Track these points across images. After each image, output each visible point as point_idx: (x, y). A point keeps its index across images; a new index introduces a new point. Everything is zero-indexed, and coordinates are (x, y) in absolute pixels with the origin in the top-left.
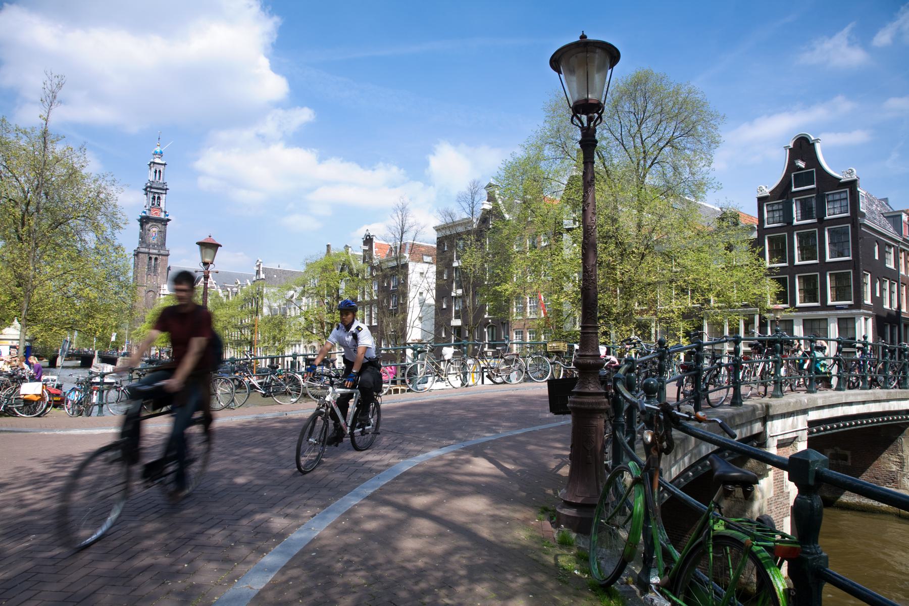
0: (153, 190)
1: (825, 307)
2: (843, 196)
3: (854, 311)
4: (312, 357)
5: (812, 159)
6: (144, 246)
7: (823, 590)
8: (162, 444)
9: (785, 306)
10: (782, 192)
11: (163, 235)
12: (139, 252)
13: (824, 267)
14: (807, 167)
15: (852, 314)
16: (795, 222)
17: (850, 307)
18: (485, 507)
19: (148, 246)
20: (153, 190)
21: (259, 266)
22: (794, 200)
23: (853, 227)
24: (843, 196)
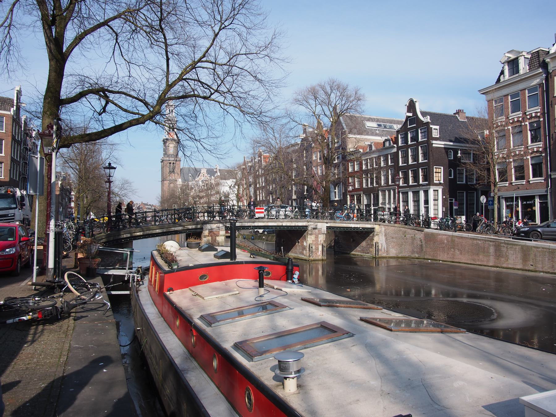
1: (409, 186)
3: (428, 187)
10: (404, 130)
12: (163, 160)
14: (413, 115)
15: (427, 188)
16: (409, 143)
17: (427, 185)
19: (168, 156)
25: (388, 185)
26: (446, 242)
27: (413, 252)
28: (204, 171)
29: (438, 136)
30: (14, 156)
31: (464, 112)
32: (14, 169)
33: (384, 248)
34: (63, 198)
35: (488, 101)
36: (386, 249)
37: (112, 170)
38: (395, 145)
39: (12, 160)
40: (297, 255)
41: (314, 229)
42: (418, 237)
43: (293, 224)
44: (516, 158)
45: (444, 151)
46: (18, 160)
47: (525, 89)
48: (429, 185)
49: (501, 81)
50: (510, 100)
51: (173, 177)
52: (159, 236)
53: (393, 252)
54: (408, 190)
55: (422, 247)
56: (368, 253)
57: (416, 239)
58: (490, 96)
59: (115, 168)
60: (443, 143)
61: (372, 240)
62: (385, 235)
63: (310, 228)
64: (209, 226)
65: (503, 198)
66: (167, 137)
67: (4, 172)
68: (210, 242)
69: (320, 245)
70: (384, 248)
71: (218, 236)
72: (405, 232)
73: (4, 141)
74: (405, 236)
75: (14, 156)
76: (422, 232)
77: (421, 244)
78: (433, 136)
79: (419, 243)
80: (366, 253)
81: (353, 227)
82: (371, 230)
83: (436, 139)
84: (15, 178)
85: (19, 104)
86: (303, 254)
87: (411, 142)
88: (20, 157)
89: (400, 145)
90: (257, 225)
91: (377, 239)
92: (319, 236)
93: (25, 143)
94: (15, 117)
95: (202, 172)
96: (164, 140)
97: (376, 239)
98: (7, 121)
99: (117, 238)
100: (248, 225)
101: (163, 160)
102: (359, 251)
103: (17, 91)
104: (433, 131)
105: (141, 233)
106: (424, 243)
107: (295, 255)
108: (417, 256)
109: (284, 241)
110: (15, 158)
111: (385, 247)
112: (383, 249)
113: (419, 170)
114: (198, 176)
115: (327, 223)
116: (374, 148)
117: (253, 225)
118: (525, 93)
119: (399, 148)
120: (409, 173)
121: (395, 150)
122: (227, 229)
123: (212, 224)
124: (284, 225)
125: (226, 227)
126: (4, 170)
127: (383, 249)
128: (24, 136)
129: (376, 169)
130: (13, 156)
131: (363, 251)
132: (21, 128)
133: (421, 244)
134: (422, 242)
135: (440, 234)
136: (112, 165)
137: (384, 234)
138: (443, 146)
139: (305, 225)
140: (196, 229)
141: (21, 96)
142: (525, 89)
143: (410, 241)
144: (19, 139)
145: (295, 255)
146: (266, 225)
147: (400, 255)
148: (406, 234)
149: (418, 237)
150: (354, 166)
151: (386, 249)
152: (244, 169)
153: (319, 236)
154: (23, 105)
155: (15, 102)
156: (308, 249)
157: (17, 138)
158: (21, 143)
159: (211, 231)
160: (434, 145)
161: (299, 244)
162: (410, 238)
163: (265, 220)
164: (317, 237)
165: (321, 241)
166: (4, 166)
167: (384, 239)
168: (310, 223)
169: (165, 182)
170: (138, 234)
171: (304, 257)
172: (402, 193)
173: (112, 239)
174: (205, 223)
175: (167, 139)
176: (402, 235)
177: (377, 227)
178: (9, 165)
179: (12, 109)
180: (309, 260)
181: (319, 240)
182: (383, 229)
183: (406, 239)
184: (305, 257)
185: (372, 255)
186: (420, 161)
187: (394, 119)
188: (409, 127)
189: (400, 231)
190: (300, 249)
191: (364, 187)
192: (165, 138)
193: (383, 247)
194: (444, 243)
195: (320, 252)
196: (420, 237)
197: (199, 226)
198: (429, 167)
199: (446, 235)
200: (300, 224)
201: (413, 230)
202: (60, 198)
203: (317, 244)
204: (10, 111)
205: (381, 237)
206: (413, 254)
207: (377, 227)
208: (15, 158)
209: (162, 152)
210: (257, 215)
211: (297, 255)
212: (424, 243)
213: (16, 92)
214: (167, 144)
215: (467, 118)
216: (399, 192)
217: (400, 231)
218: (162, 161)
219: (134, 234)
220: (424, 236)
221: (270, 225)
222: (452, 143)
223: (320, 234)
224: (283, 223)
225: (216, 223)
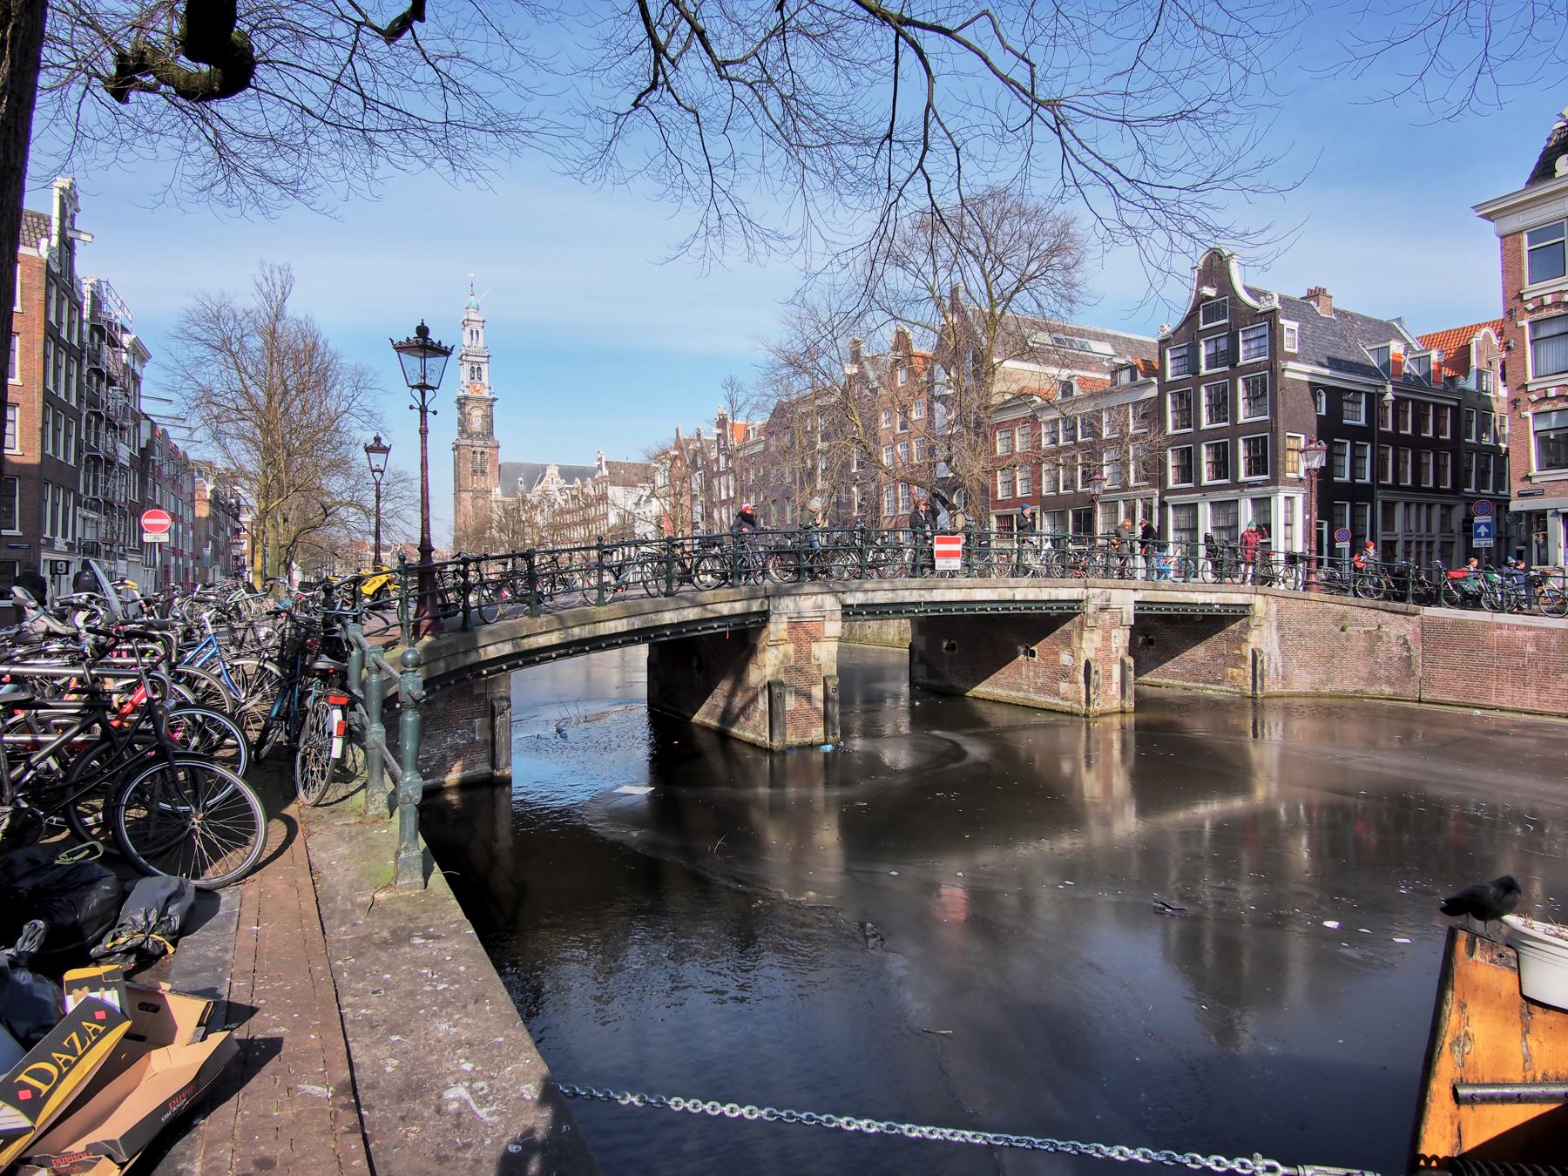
0: (469, 358)
1: (1200, 488)
2: (1261, 332)
3: (1270, 488)
4: (1100, 528)
5: (1226, 286)
6: (465, 436)
7: (460, 909)
8: (764, 650)
9: (1264, 477)
10: (1188, 334)
11: (489, 419)
12: (458, 446)
13: (1237, 430)
14: (1219, 295)
15: (1266, 492)
16: (1203, 371)
17: (1266, 483)
18: (446, 780)
19: (470, 436)
20: (469, 358)
21: (600, 459)
22: (1202, 343)
23: (1271, 373)
24: (1261, 332)
25: (1125, 487)
26: (1530, 649)
27: (1373, 678)
28: (552, 471)
29: (1296, 351)
30: (56, 387)
31: (1328, 293)
32: (56, 430)
33: (1276, 668)
34: (218, 528)
35: (1503, 237)
36: (1280, 670)
37: (434, 363)
38: (1154, 380)
39: (49, 399)
40: (1021, 694)
41: (1103, 609)
42: (1393, 633)
43: (1044, 594)
44: (1545, 407)
45: (1307, 391)
46: (73, 403)
47: (1521, 232)
48: (1274, 481)
49: (1557, 175)
50: (1526, 247)
51: (480, 483)
52: (617, 645)
53: (1303, 682)
54: (1235, 495)
55: (1410, 665)
56: (1218, 682)
57: (1385, 639)
58: (1512, 223)
59: (446, 353)
60: (1309, 368)
61: (1241, 640)
62: (1280, 627)
63: (1090, 609)
64: (787, 604)
65: (1556, 513)
66: (467, 393)
67: (21, 435)
68: (792, 663)
69: (1115, 662)
70: (1276, 668)
71: (817, 640)
72: (1343, 617)
73: (17, 338)
74: (1343, 630)
75: (56, 387)
76: (1411, 618)
77: (1405, 654)
78: (1286, 349)
79: (1396, 650)
80: (1206, 682)
81: (1200, 602)
82: (1240, 614)
83: (1293, 357)
84: (61, 457)
85: (70, 234)
86: (1057, 694)
87: (1207, 368)
88: (80, 397)
89: (1169, 377)
90: (938, 599)
91: (1257, 639)
92: (1114, 633)
93: (96, 357)
94: (56, 269)
95: (548, 472)
96: (459, 400)
97: (1254, 639)
98: (29, 276)
99: (461, 664)
100: (913, 600)
101: (458, 446)
102: (1174, 676)
103: (62, 189)
104: (1286, 335)
105: (554, 639)
106: (1417, 651)
107: (1014, 694)
108: (1388, 690)
109: (951, 648)
110: (62, 395)
111: (1280, 665)
112: (1272, 671)
113: (1200, 449)
114: (539, 483)
115: (1135, 590)
116: (1077, 391)
117: (929, 599)
118: (1520, 241)
119: (1164, 387)
120: (1199, 459)
121: (1152, 392)
122: (847, 614)
123: (800, 595)
124: (1018, 597)
125: (844, 606)
126: (21, 429)
127: (1272, 671)
128: (92, 337)
129: (1083, 446)
130: (51, 387)
131: (1195, 675)
132: (81, 310)
133: (1405, 654)
134: (1409, 650)
135: (1500, 626)
136: (434, 336)
137: (1275, 624)
138: (1306, 378)
139: (1075, 598)
140: (746, 615)
141: (78, 210)
142: (1521, 232)
143: (1362, 644)
144: (75, 342)
145: (1014, 694)
146: (968, 598)
147: (1326, 690)
148: (1346, 623)
149: (1393, 633)
150: (1012, 438)
151: (1280, 670)
152: (676, 457)
153: (1114, 633)
154: (83, 237)
155: (56, 223)
156: (1081, 678)
157: (64, 335)
158: (82, 357)
159: (795, 624)
160: (1288, 374)
161: (1036, 659)
162: (1363, 636)
163: (955, 581)
164: (1107, 638)
165: (1117, 649)
166: (21, 415)
167: (1275, 636)
168: (1092, 591)
169: (463, 495)
170: (543, 641)
171: (1060, 702)
172: (1174, 506)
173: (441, 668)
174: (779, 593)
175: (466, 398)
176: (1332, 626)
177: (1258, 602)
178: (38, 415)
179: (44, 242)
180: (1086, 716)
181: (1114, 645)
182: (1274, 607)
183: (1347, 640)
184: (1068, 703)
185: (1237, 690)
186: (1241, 419)
187: (1087, 327)
188: (1202, 327)
189: (1326, 613)
190: (1037, 675)
191: (1044, 493)
192: (461, 394)
193: (1272, 665)
194: (1521, 655)
195: (1114, 686)
196: (1402, 632)
197: (755, 606)
198: (1274, 433)
199: (1530, 628)
200: (1064, 594)
201: (1372, 612)
202: (211, 525)
203: (1108, 660)
204: (38, 247)
205: (1266, 633)
206: (1371, 685)
207: (1258, 602)
208: (62, 395)
209: (456, 428)
210: (940, 564)
211: (1021, 694)
212: (1417, 651)
213: (56, 193)
214: (467, 409)
215: (1335, 311)
216: (1163, 505)
217: (1326, 613)
218: (457, 447)
219: (525, 641)
220: (1418, 630)
221: (978, 598)
222: (1327, 372)
223: (1113, 626)
224: (1016, 591)
225: (814, 594)
